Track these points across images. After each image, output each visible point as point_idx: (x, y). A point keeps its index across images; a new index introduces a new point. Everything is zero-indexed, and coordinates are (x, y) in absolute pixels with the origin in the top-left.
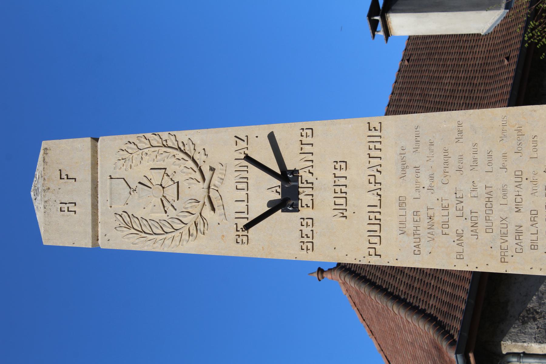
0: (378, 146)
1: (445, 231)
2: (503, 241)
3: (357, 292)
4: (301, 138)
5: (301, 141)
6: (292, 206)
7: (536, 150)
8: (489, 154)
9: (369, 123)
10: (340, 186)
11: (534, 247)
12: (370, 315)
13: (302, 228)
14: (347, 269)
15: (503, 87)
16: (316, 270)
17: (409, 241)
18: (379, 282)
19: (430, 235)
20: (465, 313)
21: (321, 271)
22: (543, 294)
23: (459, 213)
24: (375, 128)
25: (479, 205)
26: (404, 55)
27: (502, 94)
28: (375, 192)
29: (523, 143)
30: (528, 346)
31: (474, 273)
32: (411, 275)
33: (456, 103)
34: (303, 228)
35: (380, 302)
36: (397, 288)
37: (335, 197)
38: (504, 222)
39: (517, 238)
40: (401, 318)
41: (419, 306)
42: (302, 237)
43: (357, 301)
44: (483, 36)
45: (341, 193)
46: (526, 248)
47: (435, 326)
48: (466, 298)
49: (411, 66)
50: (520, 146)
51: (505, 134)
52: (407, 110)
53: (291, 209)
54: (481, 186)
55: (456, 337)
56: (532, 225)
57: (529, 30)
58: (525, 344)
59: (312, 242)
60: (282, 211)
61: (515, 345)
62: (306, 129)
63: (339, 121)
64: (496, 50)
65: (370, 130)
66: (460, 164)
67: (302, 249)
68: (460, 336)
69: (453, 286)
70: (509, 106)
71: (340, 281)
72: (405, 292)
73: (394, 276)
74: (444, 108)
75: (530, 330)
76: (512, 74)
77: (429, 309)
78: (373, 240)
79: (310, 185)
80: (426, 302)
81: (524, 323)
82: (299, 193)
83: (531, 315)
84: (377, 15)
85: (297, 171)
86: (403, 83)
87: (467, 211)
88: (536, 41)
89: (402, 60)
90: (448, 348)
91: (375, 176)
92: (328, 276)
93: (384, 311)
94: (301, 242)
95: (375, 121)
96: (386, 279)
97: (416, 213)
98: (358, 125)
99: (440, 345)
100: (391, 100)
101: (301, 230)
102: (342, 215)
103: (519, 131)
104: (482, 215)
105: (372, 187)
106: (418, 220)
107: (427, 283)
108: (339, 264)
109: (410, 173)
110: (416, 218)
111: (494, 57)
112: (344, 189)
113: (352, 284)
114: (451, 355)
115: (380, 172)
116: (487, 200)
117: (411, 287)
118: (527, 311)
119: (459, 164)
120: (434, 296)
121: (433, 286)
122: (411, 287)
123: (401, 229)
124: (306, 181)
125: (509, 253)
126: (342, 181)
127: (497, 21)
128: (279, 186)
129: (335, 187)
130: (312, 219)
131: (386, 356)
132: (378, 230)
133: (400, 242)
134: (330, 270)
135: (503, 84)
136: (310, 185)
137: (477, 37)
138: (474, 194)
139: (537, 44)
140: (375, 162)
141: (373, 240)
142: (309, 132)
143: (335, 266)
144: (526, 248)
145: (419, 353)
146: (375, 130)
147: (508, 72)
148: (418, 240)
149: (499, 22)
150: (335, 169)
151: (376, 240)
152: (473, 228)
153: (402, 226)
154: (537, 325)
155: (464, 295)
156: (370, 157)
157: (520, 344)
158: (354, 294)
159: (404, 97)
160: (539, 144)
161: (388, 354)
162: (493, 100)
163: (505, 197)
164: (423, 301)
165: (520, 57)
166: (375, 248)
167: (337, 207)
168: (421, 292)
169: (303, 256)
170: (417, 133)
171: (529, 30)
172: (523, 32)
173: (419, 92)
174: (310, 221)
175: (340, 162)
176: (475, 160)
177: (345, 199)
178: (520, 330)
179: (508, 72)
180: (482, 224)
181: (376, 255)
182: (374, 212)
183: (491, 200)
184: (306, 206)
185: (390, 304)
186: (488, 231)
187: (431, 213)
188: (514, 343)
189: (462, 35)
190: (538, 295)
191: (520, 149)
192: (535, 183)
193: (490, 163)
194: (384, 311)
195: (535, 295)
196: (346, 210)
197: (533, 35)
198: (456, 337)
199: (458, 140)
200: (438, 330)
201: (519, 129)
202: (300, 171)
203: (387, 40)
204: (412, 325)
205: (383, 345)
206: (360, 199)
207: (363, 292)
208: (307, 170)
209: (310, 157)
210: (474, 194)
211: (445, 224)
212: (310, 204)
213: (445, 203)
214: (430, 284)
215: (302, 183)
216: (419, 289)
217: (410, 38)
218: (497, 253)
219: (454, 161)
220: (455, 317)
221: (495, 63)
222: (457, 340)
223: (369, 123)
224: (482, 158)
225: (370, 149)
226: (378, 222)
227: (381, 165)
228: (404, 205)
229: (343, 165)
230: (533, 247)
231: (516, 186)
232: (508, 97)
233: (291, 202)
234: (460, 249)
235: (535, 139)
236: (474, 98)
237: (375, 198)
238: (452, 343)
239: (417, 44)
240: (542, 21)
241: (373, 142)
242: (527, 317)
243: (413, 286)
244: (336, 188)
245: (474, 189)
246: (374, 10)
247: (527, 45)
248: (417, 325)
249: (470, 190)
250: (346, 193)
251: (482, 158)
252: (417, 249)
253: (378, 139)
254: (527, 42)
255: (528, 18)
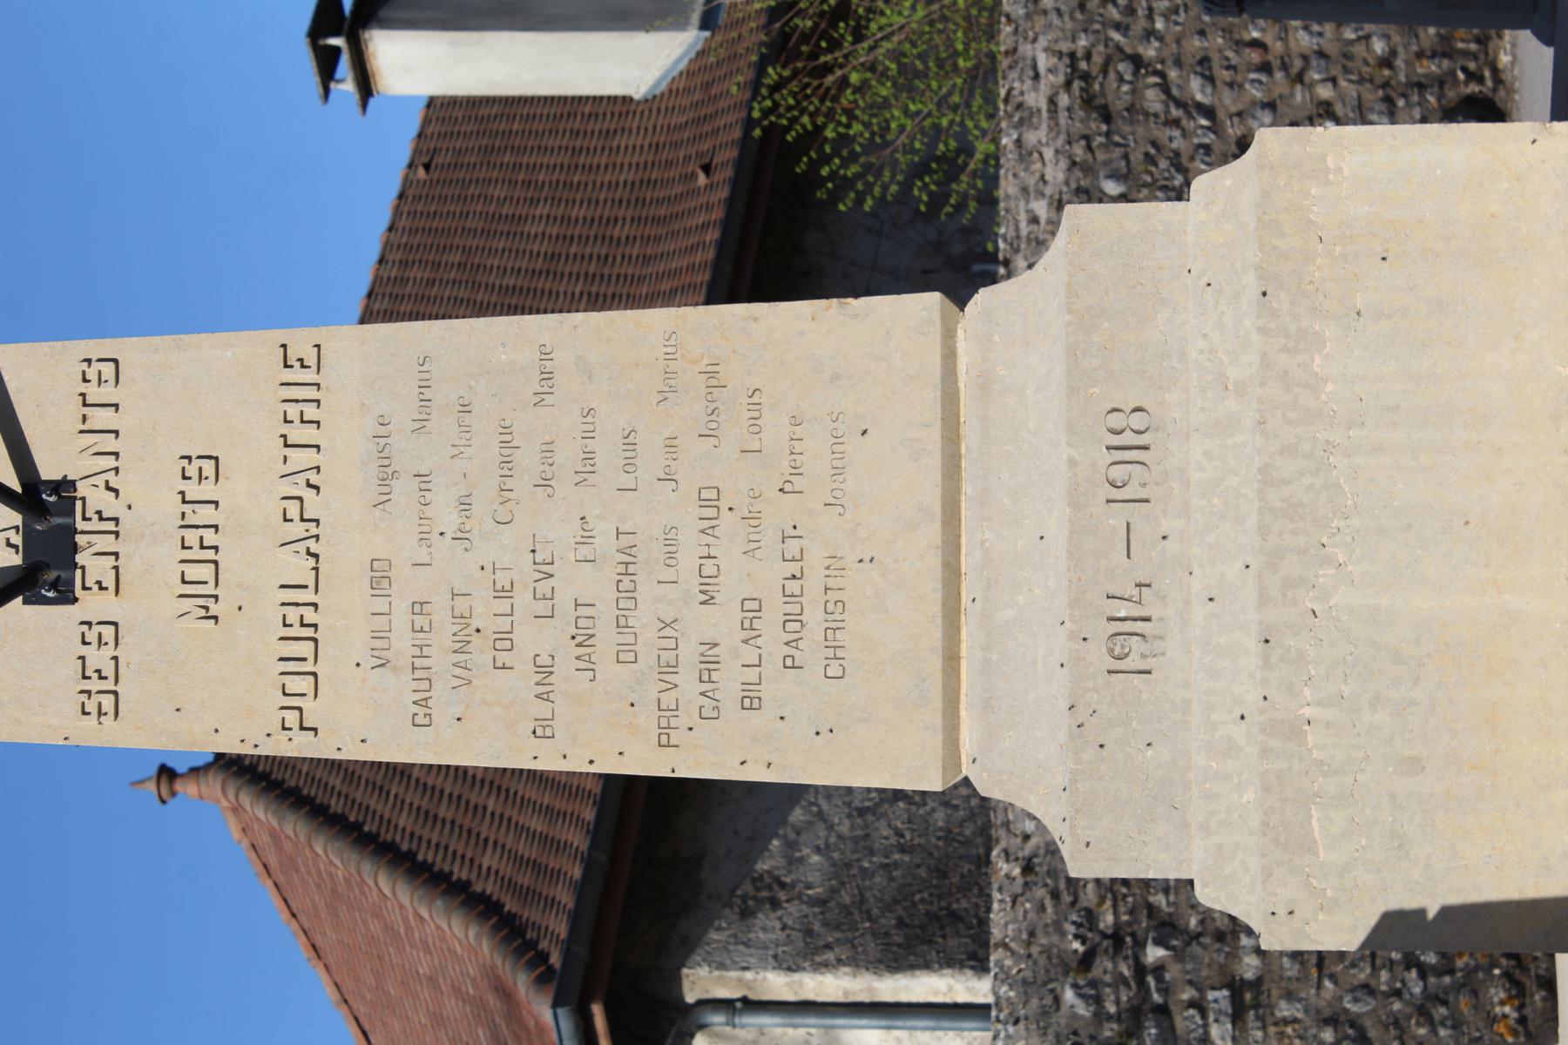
0: (311, 412)
1: (503, 658)
2: (665, 686)
3: (274, 835)
4: (83, 388)
5: (83, 395)
6: (54, 585)
7: (756, 429)
8: (629, 440)
9: (284, 346)
10: (197, 527)
11: (750, 702)
12: (313, 900)
13: (84, 650)
14: (239, 769)
15: (693, 249)
16: (153, 771)
17: (400, 688)
18: (336, 806)
19: (458, 671)
20: (581, 889)
21: (167, 774)
22: (798, 834)
23: (542, 607)
24: (301, 360)
25: (598, 585)
26: (417, 152)
27: (691, 268)
28: (301, 547)
29: (722, 408)
30: (755, 980)
31: (608, 779)
32: (430, 783)
33: (562, 291)
34: (90, 652)
35: (338, 862)
36: (389, 821)
37: (183, 561)
38: (668, 632)
39: (705, 678)
40: (401, 906)
41: (451, 873)
42: (85, 677)
43: (273, 862)
44: (639, 102)
45: (202, 547)
46: (730, 705)
47: (497, 928)
48: (584, 847)
49: (433, 184)
50: (713, 417)
51: (673, 382)
52: (514, 302)
53: (51, 594)
54: (604, 531)
55: (555, 959)
56: (746, 642)
57: (764, 91)
58: (749, 975)
59: (115, 693)
60: (25, 602)
61: (720, 978)
62: (100, 360)
63: (195, 338)
64: (675, 145)
65: (286, 366)
66: (547, 468)
67: (84, 713)
68: (567, 955)
69: (550, 813)
70: (710, 300)
71: (225, 803)
72: (412, 834)
73: (381, 788)
74: (528, 305)
75: (762, 936)
76: (718, 214)
77: (481, 881)
78: (295, 684)
79: (110, 526)
80: (472, 860)
81: (746, 914)
82: (75, 549)
83: (765, 894)
84: (336, 34)
85: (72, 485)
86: (413, 232)
87: (564, 600)
88: (785, 122)
89: (410, 166)
90: (532, 992)
91: (300, 499)
92: (188, 789)
93: (350, 888)
94: (82, 692)
95: (301, 342)
96: (359, 795)
97: (419, 607)
98: (249, 352)
99: (510, 983)
100: (377, 280)
101: (82, 658)
102: (203, 613)
103: (712, 374)
104: (606, 614)
105: (298, 529)
106: (426, 628)
107: (476, 807)
108: (219, 756)
109: (404, 490)
110: (420, 621)
111: (669, 164)
112: (210, 537)
113: (260, 811)
114: (542, 1009)
115: (317, 488)
116: (621, 569)
117: (430, 817)
118: (754, 880)
119: (542, 468)
120: (495, 843)
121: (493, 814)
122: (430, 817)
123: (376, 653)
124: (99, 513)
125: (683, 721)
126: (205, 514)
127: (678, 61)
128: (17, 528)
129: (185, 532)
130: (115, 624)
131: (357, 1020)
132: (310, 654)
133: (374, 690)
134: (195, 771)
135: (692, 240)
136: (110, 526)
137: (620, 105)
138: (584, 552)
139: (787, 130)
140: (301, 458)
141: (295, 684)
142: (107, 369)
143: (210, 759)
144: (730, 705)
145: (451, 1006)
146: (303, 366)
147: (708, 207)
148: (425, 685)
149: (682, 66)
150: (184, 478)
151: (305, 684)
152: (581, 651)
153: (378, 644)
154: (780, 919)
155: (579, 840)
156: (286, 445)
157: (733, 974)
158: (264, 839)
159: (416, 273)
160: (766, 413)
161: (362, 1011)
162: (665, 286)
163: (673, 562)
164: (463, 857)
165: (739, 164)
166: (300, 709)
167: (190, 590)
168: (457, 831)
169: (89, 733)
170: (423, 376)
171: (764, 91)
172: (748, 95)
173: (456, 258)
174: (108, 632)
175: (200, 457)
176: (589, 456)
177: (212, 566)
178: (735, 936)
179: (708, 207)
180: (606, 636)
181: (302, 728)
182: (297, 604)
183: (631, 569)
184: (96, 587)
185: (367, 867)
186: (622, 657)
187: (462, 605)
188: (716, 973)
189: (578, 100)
190: (785, 837)
191: (714, 425)
192: (753, 522)
193: (629, 465)
194: (350, 888)
195: (776, 835)
196: (216, 597)
197: (776, 105)
198: (555, 959)
199: (540, 399)
200: (506, 940)
201: (710, 369)
202: (79, 485)
203: (364, 105)
204: (430, 928)
205: (348, 985)
206: (258, 566)
207: (291, 834)
208: (100, 480)
209: (109, 443)
210: (584, 552)
211: (504, 641)
212: (109, 582)
213: (503, 579)
214: (485, 808)
215: (84, 519)
216: (453, 822)
217: (432, 102)
218: (647, 719)
219: (528, 458)
220: (552, 903)
221: (671, 182)
222: (558, 966)
223: (284, 346)
224: (607, 450)
225: (286, 421)
226: (309, 632)
227: (318, 468)
228: (385, 584)
229: (209, 467)
230: (747, 702)
231: (703, 531)
232: (707, 276)
233: (52, 575)
234: (544, 709)
235: (755, 399)
236: (614, 278)
237: (303, 562)
238: (544, 978)
239: (449, 119)
240: (800, 65)
241: (297, 401)
242: (754, 898)
243: (436, 816)
244: (188, 533)
245: (586, 540)
246: (326, 20)
247: (757, 132)
248: (445, 927)
249: (572, 541)
250: (216, 548)
251: (607, 450)
252: (421, 711)
253: (310, 393)
254: (757, 123)
255: (762, 56)
